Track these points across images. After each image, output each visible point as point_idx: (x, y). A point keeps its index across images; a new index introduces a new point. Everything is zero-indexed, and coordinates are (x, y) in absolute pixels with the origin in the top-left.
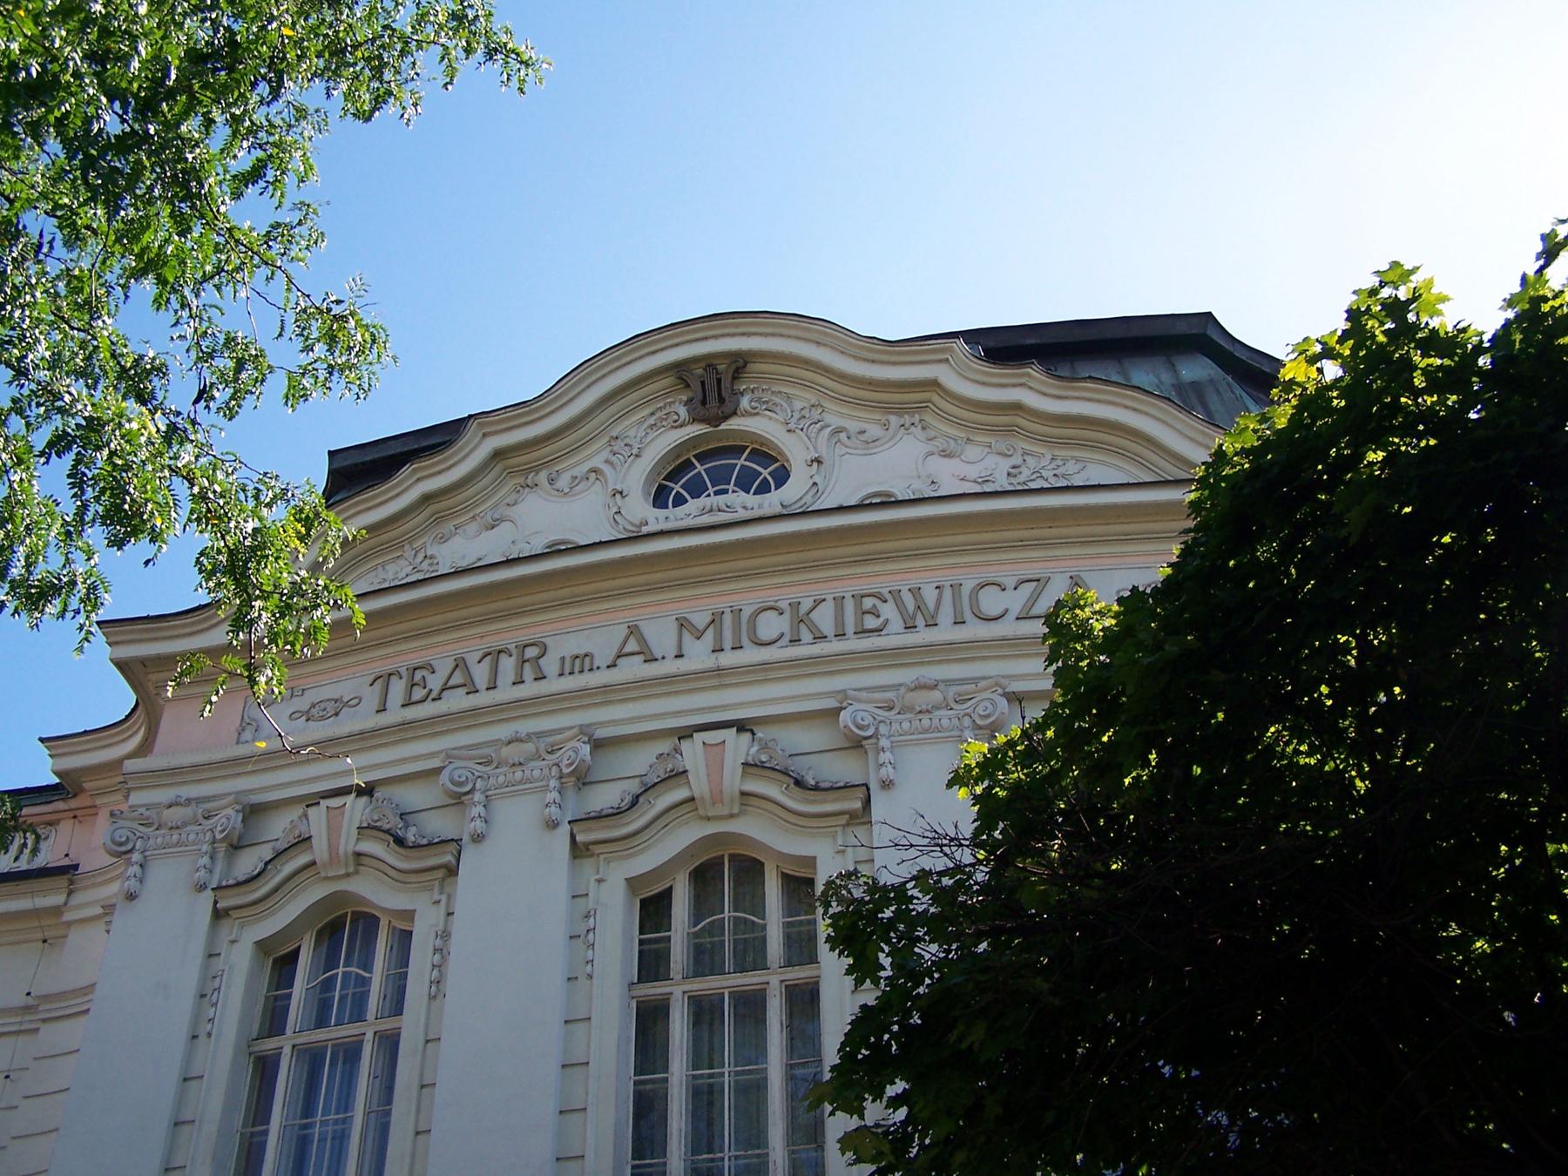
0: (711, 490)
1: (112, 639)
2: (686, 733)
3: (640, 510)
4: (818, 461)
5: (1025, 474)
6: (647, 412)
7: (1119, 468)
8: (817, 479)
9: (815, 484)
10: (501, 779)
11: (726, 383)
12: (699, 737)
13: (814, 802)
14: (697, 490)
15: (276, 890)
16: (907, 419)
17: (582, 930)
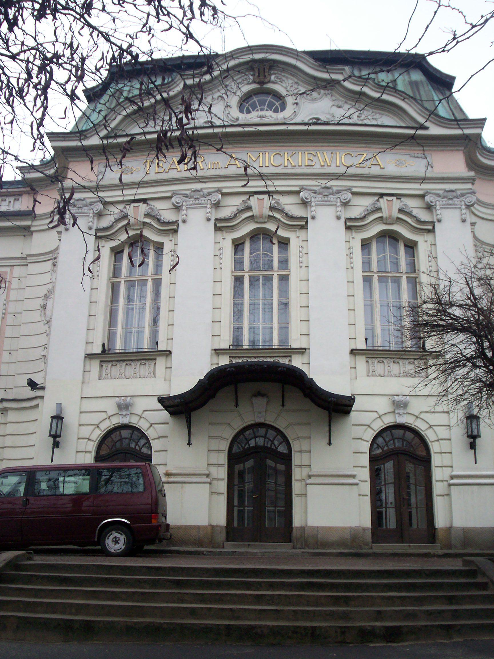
0: (259, 108)
1: (51, 139)
3: (235, 113)
4: (297, 104)
8: (296, 110)
9: (295, 112)
10: (191, 202)
11: (267, 70)
12: (256, 196)
13: (291, 221)
14: (254, 107)
15: (116, 231)
16: (326, 92)
17: (218, 253)
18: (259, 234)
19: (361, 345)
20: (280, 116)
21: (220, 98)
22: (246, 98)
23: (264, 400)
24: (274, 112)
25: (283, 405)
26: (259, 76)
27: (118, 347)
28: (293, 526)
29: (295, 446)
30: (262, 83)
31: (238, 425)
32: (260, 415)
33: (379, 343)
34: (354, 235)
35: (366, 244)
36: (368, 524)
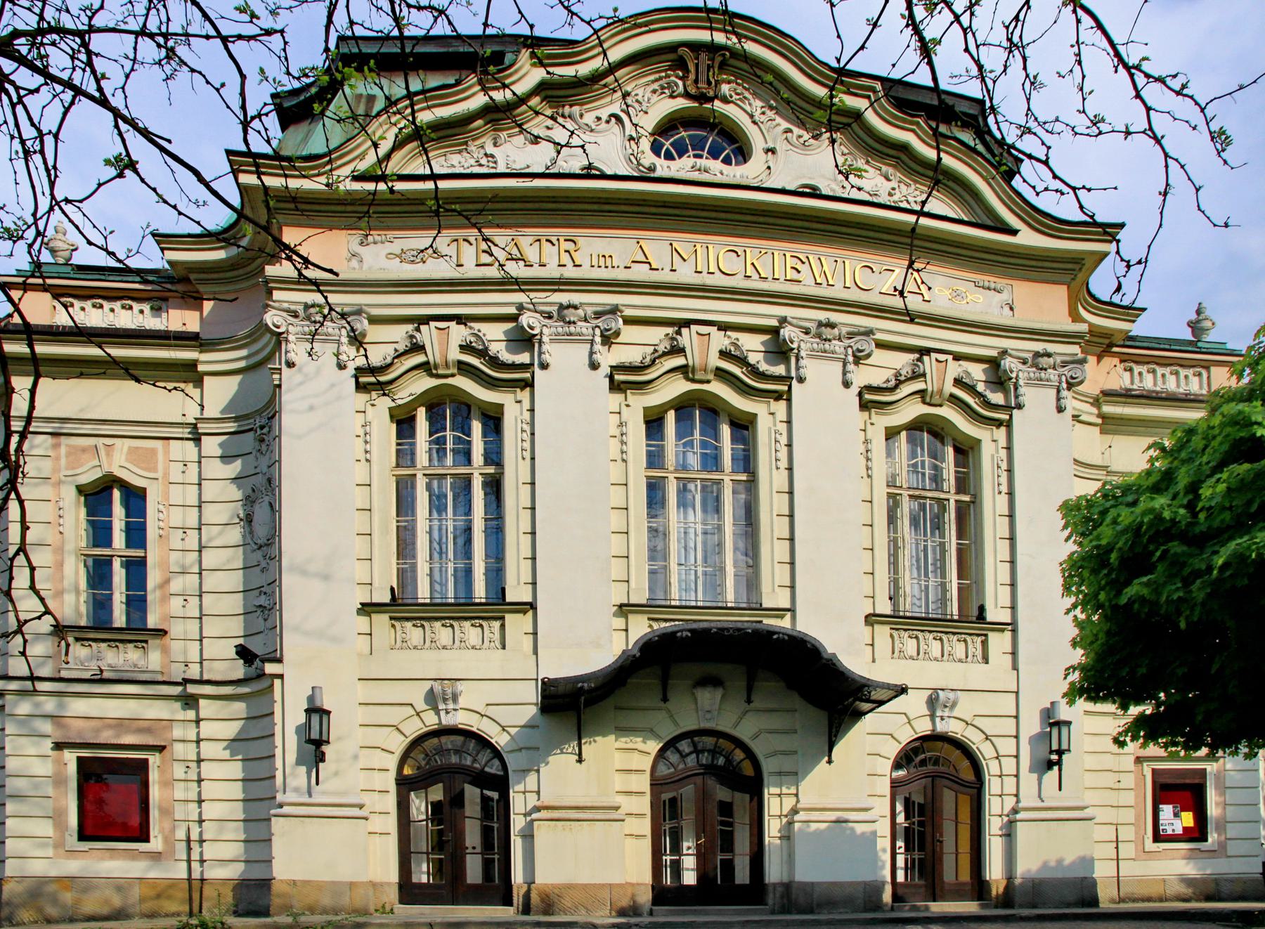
0: (691, 153)
2: (687, 323)
5: (896, 198)
6: (652, 78)
7: (952, 209)
8: (771, 164)
18: (694, 406)
19: (885, 607)
20: (735, 173)
21: (613, 120)
22: (667, 127)
23: (719, 693)
24: (724, 161)
25: (749, 701)
26: (696, 81)
27: (423, 593)
28: (767, 881)
29: (767, 766)
30: (702, 98)
31: (670, 732)
32: (708, 716)
33: (909, 606)
34: (875, 418)
35: (654, 423)
36: (647, 878)
